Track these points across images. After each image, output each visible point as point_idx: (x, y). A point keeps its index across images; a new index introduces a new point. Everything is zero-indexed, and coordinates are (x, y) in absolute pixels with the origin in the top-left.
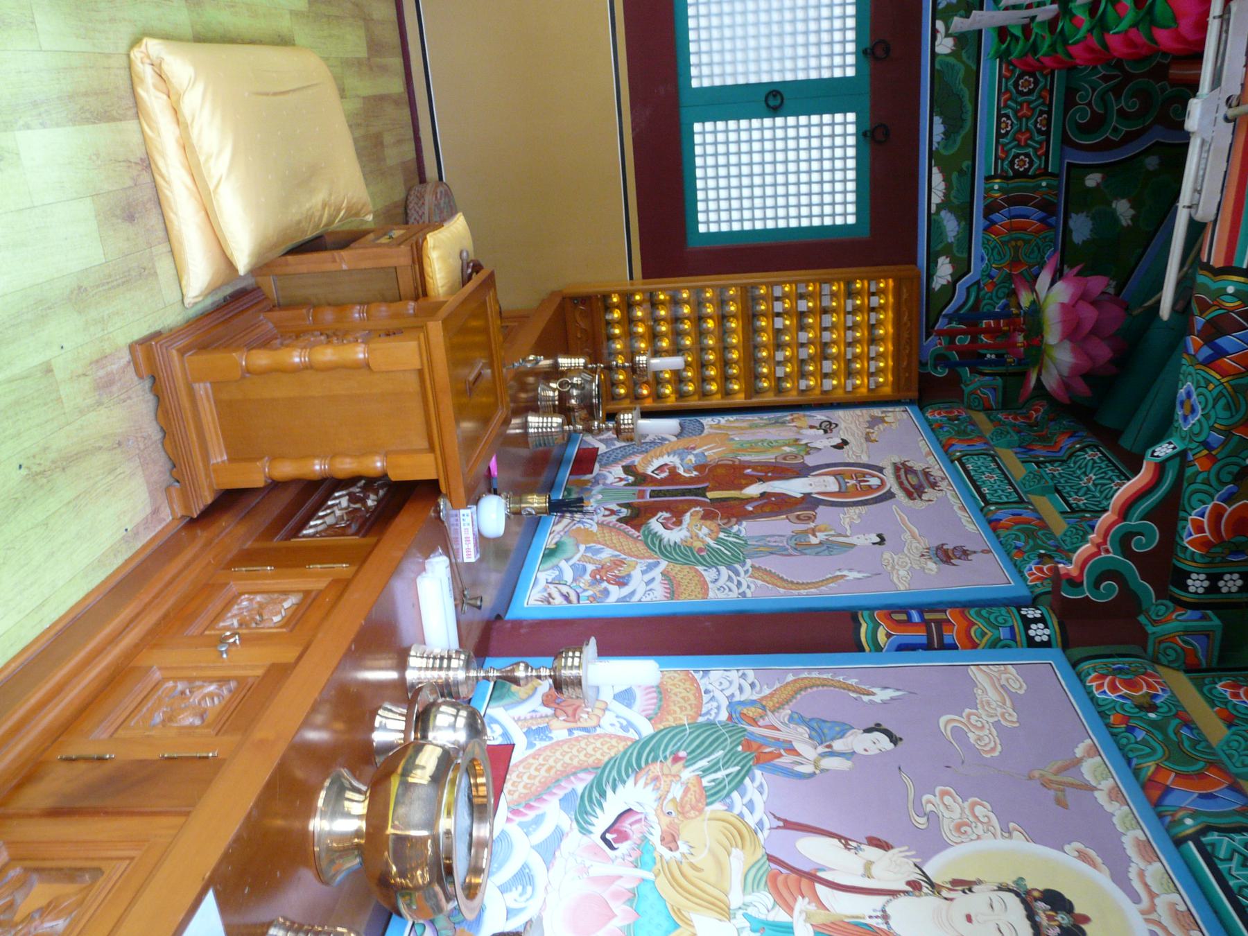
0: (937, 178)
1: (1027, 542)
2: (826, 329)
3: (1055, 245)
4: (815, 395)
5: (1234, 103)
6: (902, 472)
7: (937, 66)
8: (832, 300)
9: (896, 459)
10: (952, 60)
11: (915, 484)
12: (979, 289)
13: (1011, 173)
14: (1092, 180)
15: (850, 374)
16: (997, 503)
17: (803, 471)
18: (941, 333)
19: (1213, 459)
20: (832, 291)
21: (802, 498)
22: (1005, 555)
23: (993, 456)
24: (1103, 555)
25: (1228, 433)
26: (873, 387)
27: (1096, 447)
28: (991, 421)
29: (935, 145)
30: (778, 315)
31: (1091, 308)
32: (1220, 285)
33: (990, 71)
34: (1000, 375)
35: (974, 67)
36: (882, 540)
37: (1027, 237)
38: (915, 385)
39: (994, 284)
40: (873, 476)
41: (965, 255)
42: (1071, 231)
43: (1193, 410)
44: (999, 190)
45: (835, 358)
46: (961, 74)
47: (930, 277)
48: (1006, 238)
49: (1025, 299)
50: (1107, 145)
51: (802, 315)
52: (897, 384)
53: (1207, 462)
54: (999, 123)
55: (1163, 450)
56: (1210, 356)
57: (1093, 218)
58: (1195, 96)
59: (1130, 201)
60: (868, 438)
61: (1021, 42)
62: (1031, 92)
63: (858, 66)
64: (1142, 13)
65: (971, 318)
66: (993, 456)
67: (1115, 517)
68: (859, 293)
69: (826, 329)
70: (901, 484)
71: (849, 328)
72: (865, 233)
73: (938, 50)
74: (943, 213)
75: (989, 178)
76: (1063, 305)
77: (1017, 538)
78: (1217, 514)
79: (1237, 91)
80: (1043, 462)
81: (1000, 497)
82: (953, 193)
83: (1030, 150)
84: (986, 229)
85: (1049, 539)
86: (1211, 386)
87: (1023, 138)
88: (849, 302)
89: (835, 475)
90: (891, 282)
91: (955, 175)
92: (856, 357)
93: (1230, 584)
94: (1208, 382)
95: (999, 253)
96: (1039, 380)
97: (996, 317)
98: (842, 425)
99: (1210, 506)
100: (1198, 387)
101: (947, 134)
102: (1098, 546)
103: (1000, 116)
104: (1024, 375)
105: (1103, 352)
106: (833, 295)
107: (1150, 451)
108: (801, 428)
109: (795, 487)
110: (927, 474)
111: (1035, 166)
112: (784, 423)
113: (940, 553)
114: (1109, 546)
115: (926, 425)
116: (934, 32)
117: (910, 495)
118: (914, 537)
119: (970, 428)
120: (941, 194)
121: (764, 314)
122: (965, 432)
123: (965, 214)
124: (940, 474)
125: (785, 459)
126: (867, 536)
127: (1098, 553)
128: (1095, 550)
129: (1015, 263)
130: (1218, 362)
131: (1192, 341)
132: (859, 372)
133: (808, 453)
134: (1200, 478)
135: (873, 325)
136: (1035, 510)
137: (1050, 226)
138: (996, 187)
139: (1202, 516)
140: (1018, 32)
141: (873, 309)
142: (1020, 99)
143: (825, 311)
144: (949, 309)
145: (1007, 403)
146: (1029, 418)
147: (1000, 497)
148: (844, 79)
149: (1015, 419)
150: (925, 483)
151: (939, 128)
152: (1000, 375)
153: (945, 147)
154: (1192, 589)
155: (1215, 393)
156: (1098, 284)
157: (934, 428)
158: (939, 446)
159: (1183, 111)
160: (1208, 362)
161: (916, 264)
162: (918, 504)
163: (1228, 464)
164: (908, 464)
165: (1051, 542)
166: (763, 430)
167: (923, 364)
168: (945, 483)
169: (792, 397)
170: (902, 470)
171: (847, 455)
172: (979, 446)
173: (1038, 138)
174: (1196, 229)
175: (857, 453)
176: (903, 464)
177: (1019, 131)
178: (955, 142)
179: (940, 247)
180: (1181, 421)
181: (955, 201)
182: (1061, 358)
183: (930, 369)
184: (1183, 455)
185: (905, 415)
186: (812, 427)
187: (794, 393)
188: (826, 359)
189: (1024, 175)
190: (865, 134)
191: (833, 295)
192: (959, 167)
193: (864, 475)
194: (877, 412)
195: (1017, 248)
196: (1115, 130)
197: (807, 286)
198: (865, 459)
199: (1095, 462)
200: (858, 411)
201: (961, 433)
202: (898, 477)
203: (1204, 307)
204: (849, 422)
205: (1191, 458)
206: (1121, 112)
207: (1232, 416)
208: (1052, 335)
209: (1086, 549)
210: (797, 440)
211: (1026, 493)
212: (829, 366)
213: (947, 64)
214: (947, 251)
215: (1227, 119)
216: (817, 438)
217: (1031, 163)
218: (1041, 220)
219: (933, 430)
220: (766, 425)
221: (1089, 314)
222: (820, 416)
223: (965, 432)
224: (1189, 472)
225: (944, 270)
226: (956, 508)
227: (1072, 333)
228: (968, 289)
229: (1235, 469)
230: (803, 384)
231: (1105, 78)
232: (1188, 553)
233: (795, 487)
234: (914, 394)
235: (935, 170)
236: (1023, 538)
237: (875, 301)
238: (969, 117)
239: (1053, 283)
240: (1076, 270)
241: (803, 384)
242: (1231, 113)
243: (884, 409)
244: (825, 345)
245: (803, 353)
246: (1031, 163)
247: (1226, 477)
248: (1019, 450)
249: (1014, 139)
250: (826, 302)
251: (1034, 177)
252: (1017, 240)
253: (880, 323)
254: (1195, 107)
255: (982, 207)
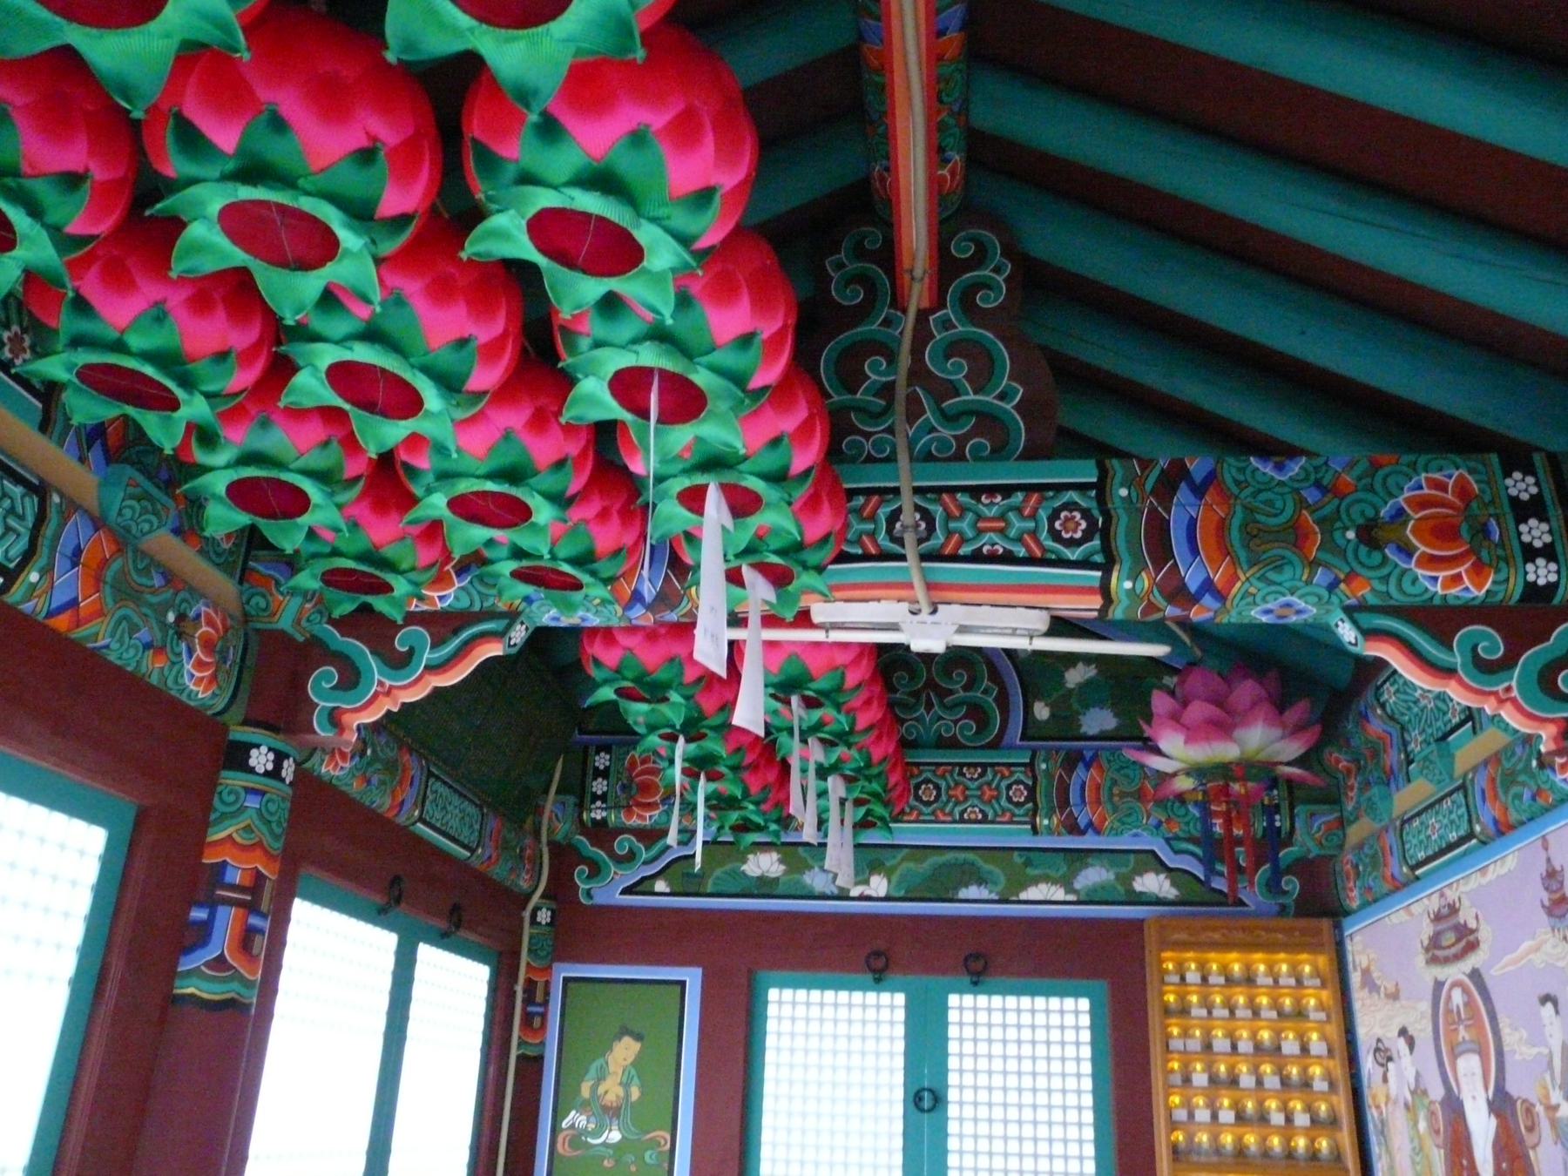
0: (1033, 893)
1: (1524, 784)
2: (1234, 1047)
3: (1120, 748)
4: (1338, 1068)
5: (916, 606)
6: (1440, 953)
7: (902, 893)
8: (1193, 1037)
9: (1421, 959)
10: (895, 878)
11: (1453, 938)
12: (1177, 838)
13: (1030, 805)
14: (1042, 711)
15: (1300, 1013)
16: (1470, 821)
17: (1453, 1107)
18: (1233, 883)
19: (1351, 577)
20: (1180, 1036)
21: (1498, 1116)
22: (1548, 816)
23: (1403, 823)
24: (1515, 693)
25: (1314, 564)
26: (1318, 982)
27: (1378, 688)
28: (1357, 818)
29: (994, 896)
30: (1215, 1116)
31: (1190, 708)
32: (1123, 597)
33: (908, 833)
34: (1292, 808)
35: (906, 851)
36: (1546, 999)
37: (1108, 784)
38: (1312, 923)
39: (1169, 820)
40: (1449, 998)
41: (1132, 857)
42: (1102, 732)
43: (1288, 605)
44: (1050, 819)
45: (1277, 1034)
46: (911, 865)
47: (1159, 902)
48: (1109, 806)
49: (1185, 784)
50: (1003, 701)
51: (1214, 1080)
52: (1314, 948)
53: (1355, 584)
54: (970, 821)
55: (1347, 633)
56: (1213, 596)
57: (1087, 707)
58: (908, 647)
59: (1067, 668)
60: (1394, 996)
61: (871, 806)
62: (937, 787)
63: (893, 990)
64: (827, 703)
65: (1214, 850)
66: (1403, 823)
67: (1453, 683)
68: (1182, 998)
69: (1234, 1047)
70: (1458, 957)
71: (1232, 1012)
72: (1101, 986)
73: (882, 893)
74: (1077, 886)
75: (1035, 831)
76: (1186, 742)
77: (1519, 796)
78: (1431, 562)
79: (905, 606)
80: (1407, 755)
81: (1460, 817)
82: (1052, 873)
83: (1004, 784)
84: (1098, 832)
85: (1513, 754)
86: (1252, 590)
87: (988, 793)
88: (1195, 1012)
89: (1454, 1057)
90: (1166, 954)
91: (1030, 871)
92: (1276, 1005)
93: (1536, 533)
94: (1247, 594)
95: (1130, 815)
96: (1289, 764)
97: (1207, 815)
98: (1379, 1032)
99: (1420, 572)
100: (1255, 603)
101: (981, 881)
102: (1501, 702)
103: (962, 821)
104: (1290, 781)
105: (1246, 691)
106: (1185, 1034)
107: (1352, 649)
108: (1388, 1097)
109: (1482, 1127)
110: (1438, 918)
111: (1022, 777)
112: (1382, 1122)
113: (1558, 912)
114: (1500, 688)
115: (1369, 909)
116: (862, 898)
117: (1473, 946)
118: (1537, 949)
119: (1366, 849)
120: (1053, 888)
121: (1215, 1138)
122: (1374, 856)
123: (1080, 857)
124: (1435, 897)
125: (1437, 1132)
126: (1546, 1022)
127: (1514, 701)
128: (1508, 705)
129: (1140, 795)
130: (1219, 587)
131: (1196, 615)
132: (1298, 1001)
133: (1425, 1093)
134: (1381, 587)
135: (1227, 980)
136: (1475, 769)
137: (1095, 757)
138: (1046, 822)
139: (1435, 579)
140: (862, 811)
141: (1204, 979)
142: (944, 798)
143: (1208, 1047)
144: (1199, 872)
145: (1331, 798)
146: (1349, 771)
147: (1460, 817)
148: (908, 1007)
149: (1352, 788)
150: (1452, 921)
151: (972, 892)
152: (1292, 808)
153: (995, 883)
154: (1553, 578)
155: (1260, 585)
156: (1160, 703)
157: (1373, 900)
158: (1398, 896)
159: (928, 657)
160: (1221, 596)
161: (1143, 921)
162: (1485, 934)
163: (1356, 557)
164: (1426, 942)
165: (1519, 750)
166: (1398, 1158)
167: (1283, 911)
168: (1448, 892)
169: (1342, 1104)
170: (1436, 952)
171: (1422, 1030)
172: (1391, 839)
173: (989, 775)
174: (1061, 626)
175: (1417, 1016)
176: (1427, 950)
177: (980, 798)
178: (990, 872)
179: (1121, 889)
180: (1304, 616)
181: (1061, 872)
182: (1260, 739)
183: (1289, 901)
184: (1350, 611)
185: (1357, 938)
186: (1385, 1080)
187: (1334, 1099)
188: (1279, 1048)
189: (1032, 790)
190: (975, 984)
191: (1185, 1034)
192: (1022, 866)
193: (1449, 1011)
194: (1355, 978)
195: (1123, 795)
196: (985, 692)
197: (1172, 1071)
198: (1425, 1006)
199: (1398, 691)
200: (1357, 1006)
201: (1376, 862)
202: (1447, 961)
203: (1151, 607)
204: (1372, 1022)
205: (1353, 601)
206: (966, 688)
207: (1290, 563)
208: (1225, 752)
209: (1508, 715)
210: (1406, 1106)
211: (1452, 778)
212: (1290, 1046)
213: (899, 883)
214: (1126, 880)
215: (934, 611)
216: (1400, 1075)
217: (1018, 782)
218: (1088, 766)
219: (1375, 901)
220: (1388, 1151)
221: (1198, 710)
222: (1368, 1064)
223: (1374, 856)
224: (1372, 600)
225: (1151, 883)
226: (1484, 881)
227: (1222, 727)
228: (1177, 852)
229: (1363, 550)
230: (1320, 1085)
231: (929, 706)
232: (1496, 588)
233: (1482, 1127)
234: (1326, 924)
235: (1023, 896)
236: (1515, 790)
237: (1193, 976)
238: (962, 856)
239: (1159, 752)
240: (1145, 727)
241: (1320, 1085)
242: (926, 609)
243: (1351, 967)
244: (1258, 1047)
245: (1272, 1082)
246: (1018, 782)
247: (1376, 558)
248: (1393, 786)
249: (989, 802)
250: (1194, 1045)
251: (1035, 778)
252: (1111, 795)
253: (1225, 971)
254: (919, 645)
255: (1070, 838)
